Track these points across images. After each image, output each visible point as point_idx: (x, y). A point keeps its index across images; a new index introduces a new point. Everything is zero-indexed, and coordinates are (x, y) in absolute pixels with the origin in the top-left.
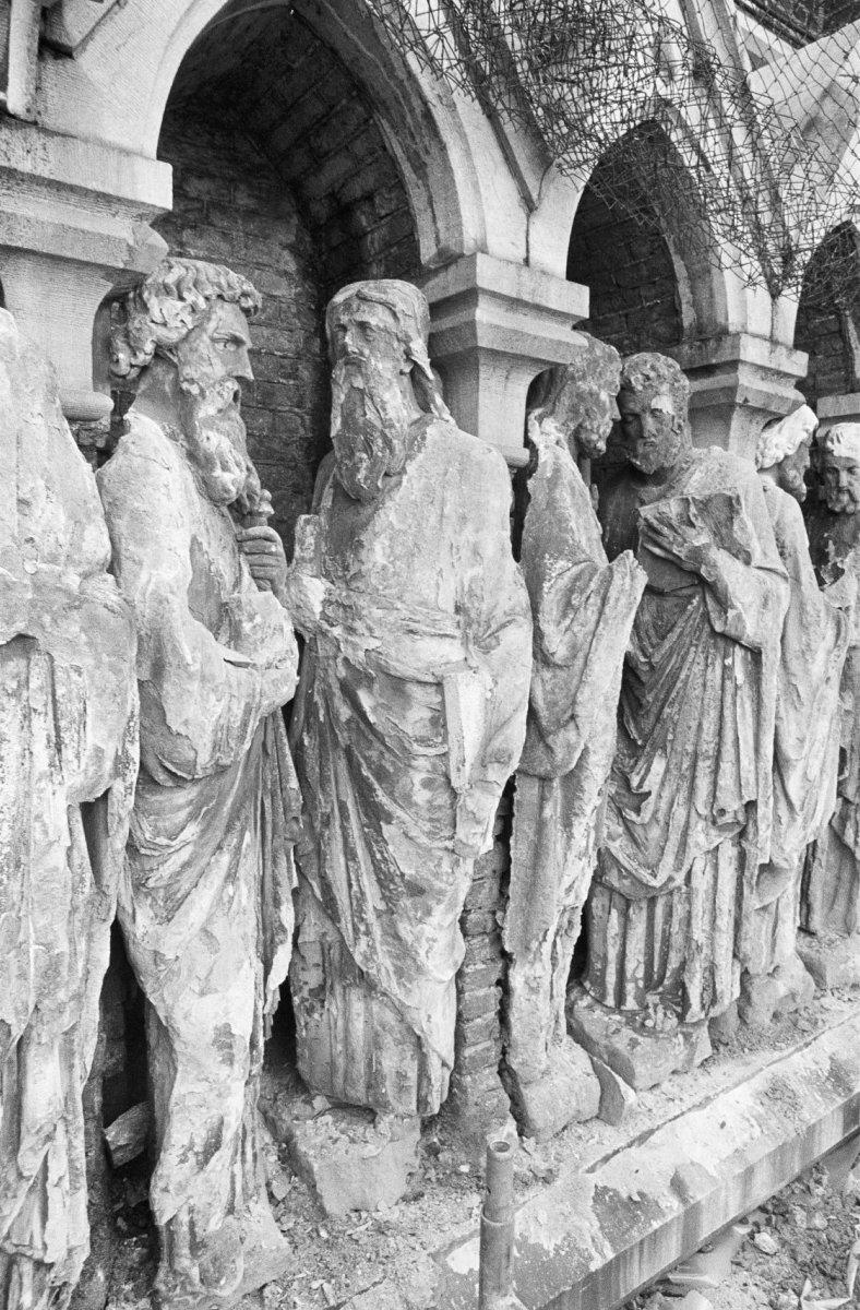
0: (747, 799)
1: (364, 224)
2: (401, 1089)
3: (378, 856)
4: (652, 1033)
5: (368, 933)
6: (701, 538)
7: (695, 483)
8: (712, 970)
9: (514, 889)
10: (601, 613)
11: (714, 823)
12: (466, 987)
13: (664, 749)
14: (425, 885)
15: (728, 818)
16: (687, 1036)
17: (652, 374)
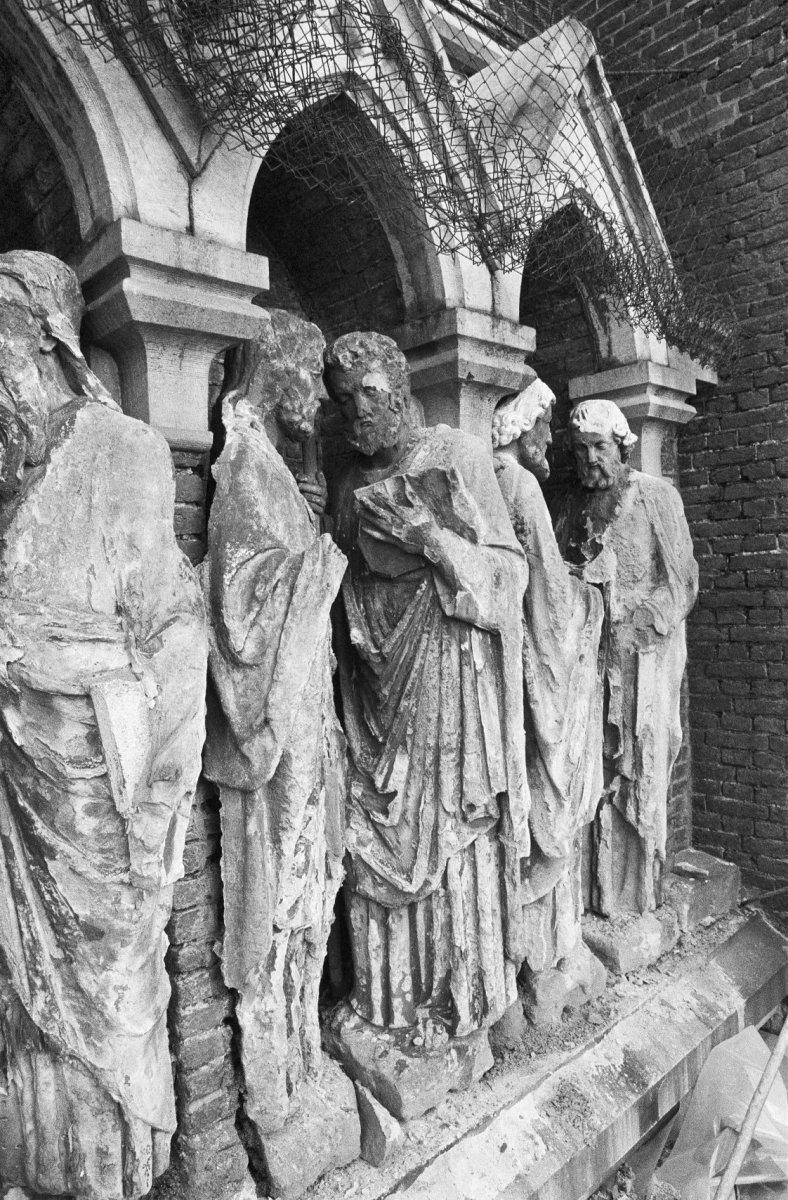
0: (497, 791)
1: (32, 203)
2: (104, 1169)
3: (48, 897)
4: (421, 1052)
5: (44, 987)
6: (420, 516)
7: (419, 461)
8: (480, 976)
9: (228, 917)
10: (289, 603)
11: (465, 819)
12: (185, 1032)
13: (404, 744)
14: (103, 927)
15: (479, 813)
16: (461, 1051)
17: (360, 351)
